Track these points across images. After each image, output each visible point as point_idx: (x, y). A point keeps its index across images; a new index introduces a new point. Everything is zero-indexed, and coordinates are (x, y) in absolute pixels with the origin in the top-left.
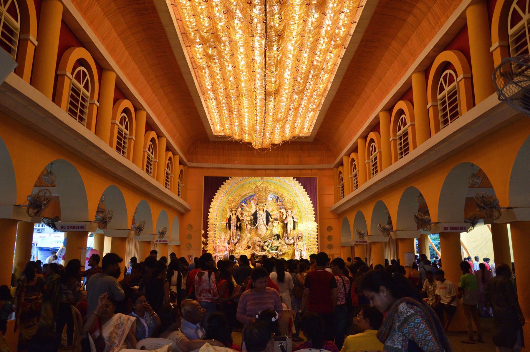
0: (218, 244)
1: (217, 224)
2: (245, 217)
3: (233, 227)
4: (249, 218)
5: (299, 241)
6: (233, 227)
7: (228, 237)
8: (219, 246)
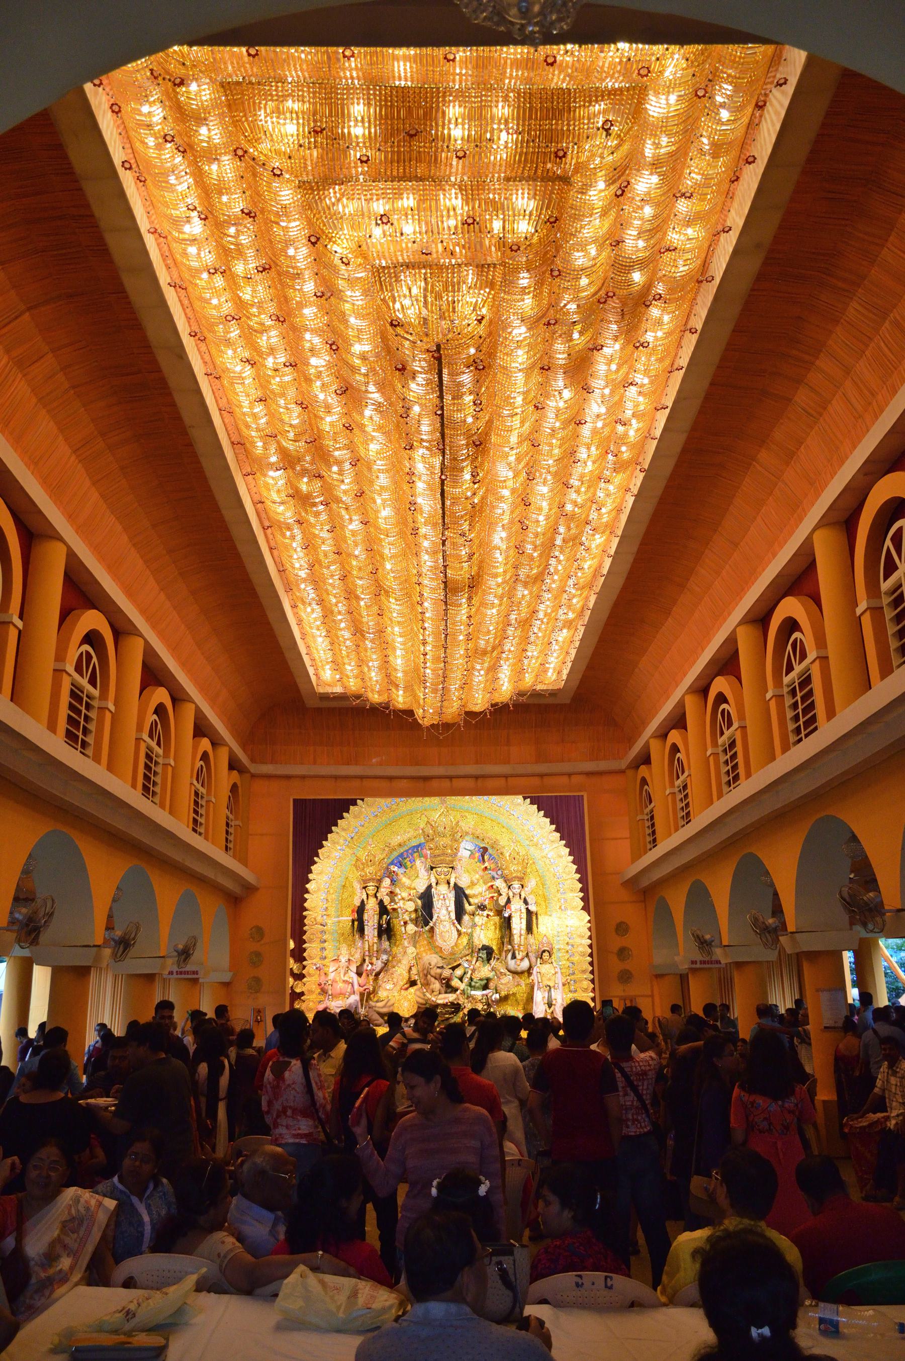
0: (331, 976)
1: (330, 922)
2: (401, 904)
3: (371, 931)
4: (411, 906)
5: (543, 962)
6: (371, 931)
7: (358, 956)
8: (334, 981)
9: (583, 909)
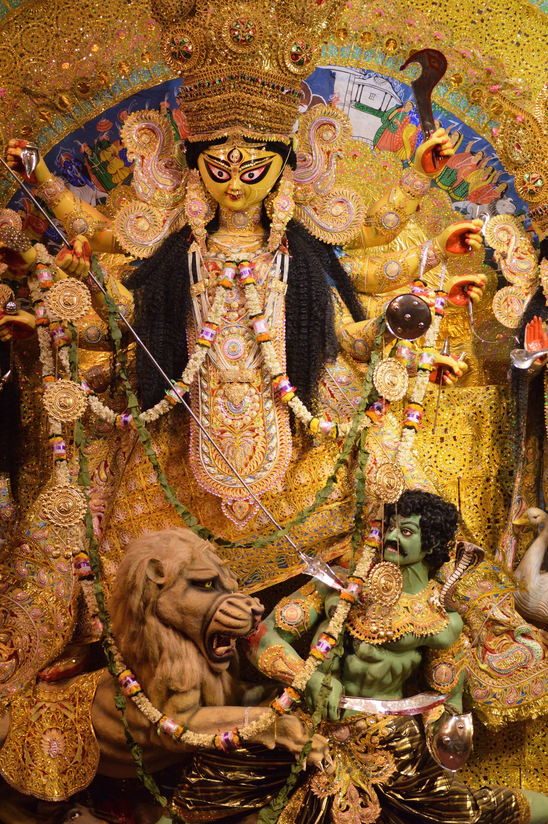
9: (193, 239)
